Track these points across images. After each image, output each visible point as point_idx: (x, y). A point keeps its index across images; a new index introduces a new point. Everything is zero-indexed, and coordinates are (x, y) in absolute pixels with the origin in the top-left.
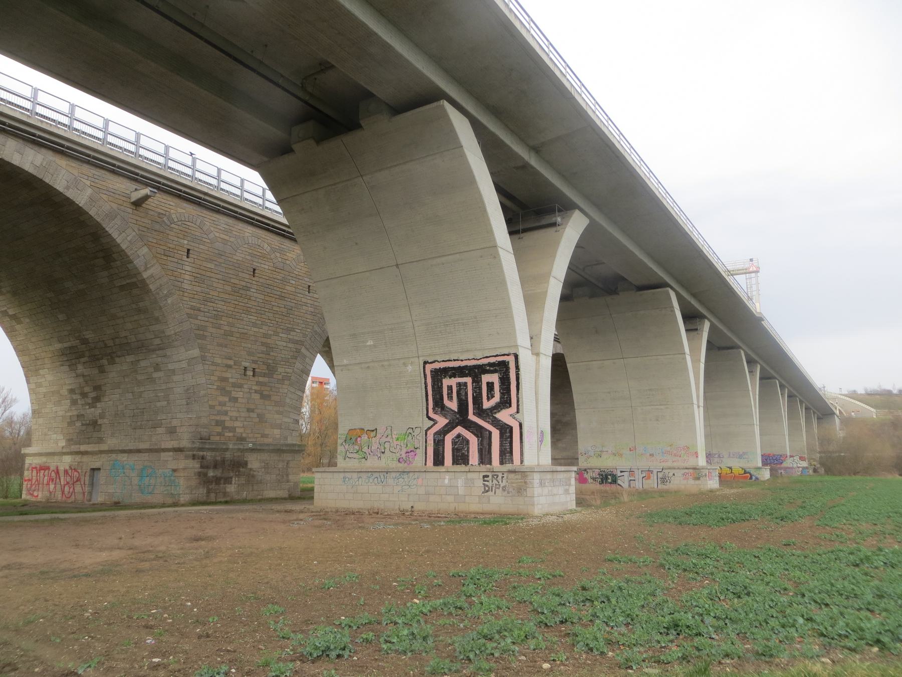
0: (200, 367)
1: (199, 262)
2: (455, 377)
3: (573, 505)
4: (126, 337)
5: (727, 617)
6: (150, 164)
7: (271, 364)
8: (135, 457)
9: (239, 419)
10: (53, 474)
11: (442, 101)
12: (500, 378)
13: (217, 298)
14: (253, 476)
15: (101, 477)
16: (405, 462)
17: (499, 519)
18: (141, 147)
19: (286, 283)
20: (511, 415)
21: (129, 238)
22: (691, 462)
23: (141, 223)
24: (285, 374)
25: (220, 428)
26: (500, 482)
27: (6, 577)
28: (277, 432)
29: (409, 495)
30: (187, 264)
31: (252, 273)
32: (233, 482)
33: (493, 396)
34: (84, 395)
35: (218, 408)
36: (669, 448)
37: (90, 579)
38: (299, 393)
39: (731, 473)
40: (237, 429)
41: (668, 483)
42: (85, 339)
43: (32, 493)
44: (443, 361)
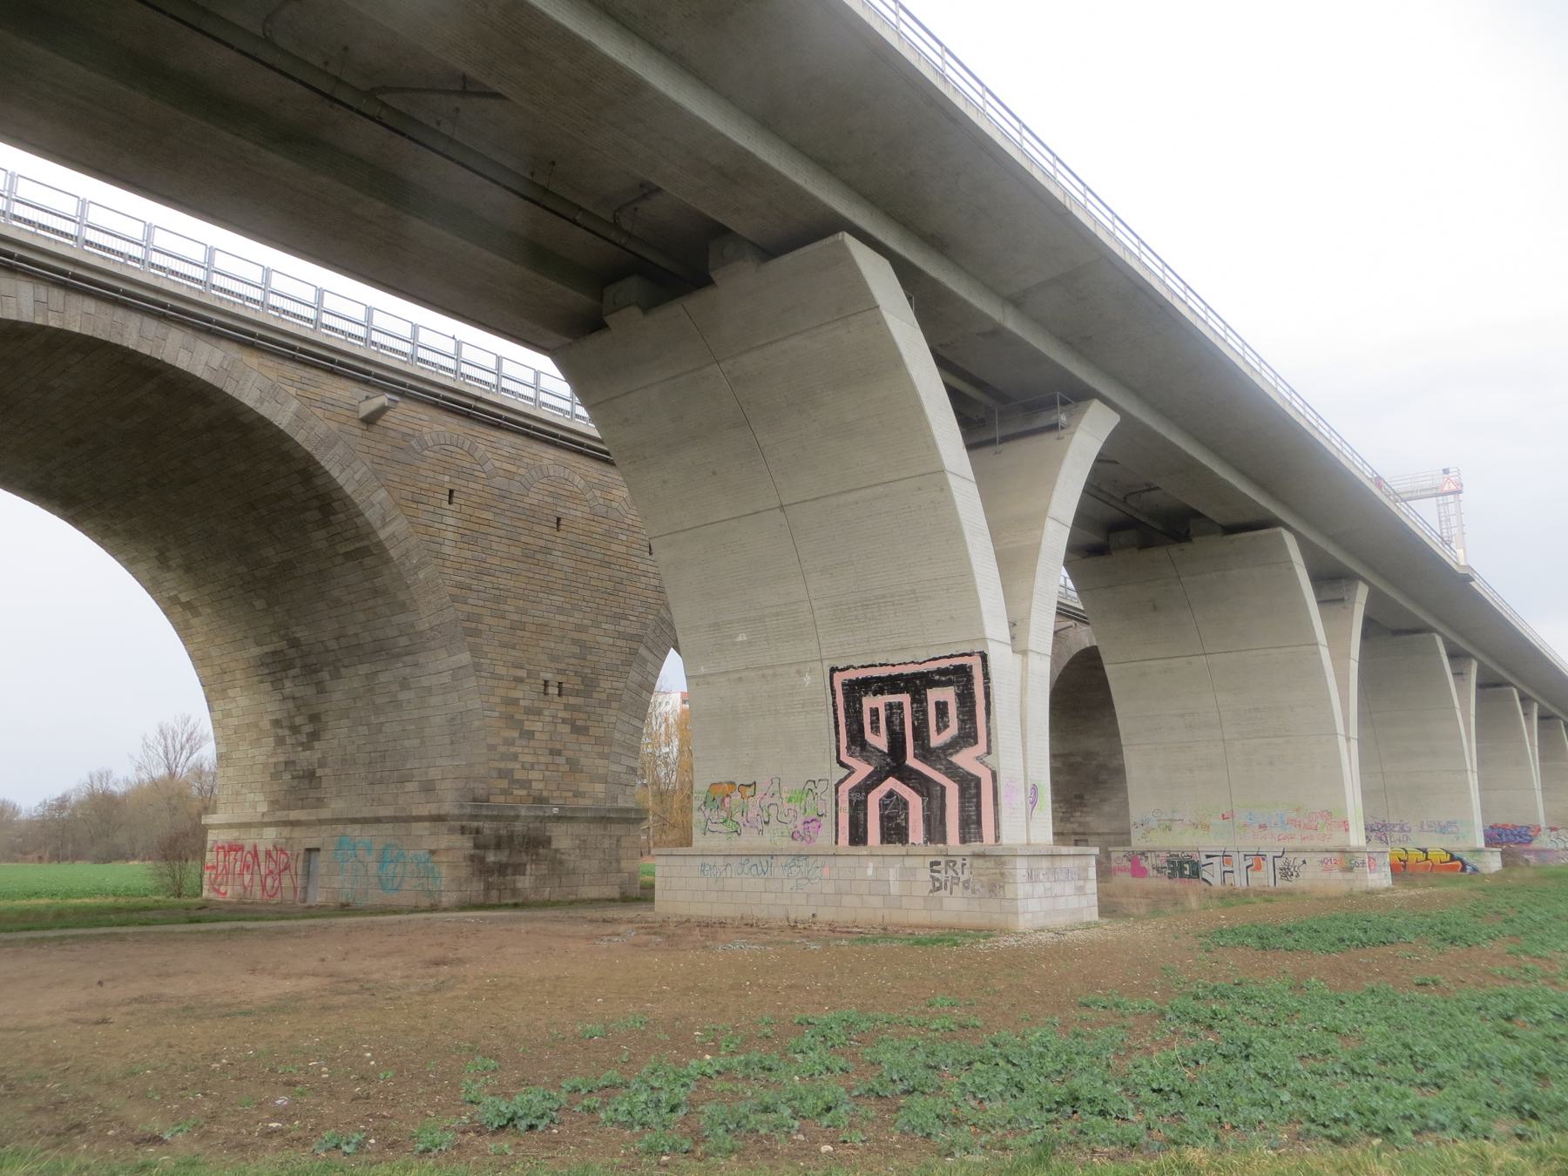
0: (471, 683)
1: (469, 511)
2: (882, 694)
3: (1093, 915)
4: (356, 635)
5: (1173, 1090)
6: (388, 356)
7: (589, 676)
8: (372, 830)
9: (536, 767)
10: (249, 858)
11: (840, 234)
12: (957, 694)
13: (498, 568)
14: (561, 862)
15: (321, 863)
16: (803, 839)
17: (949, 936)
18: (374, 329)
19: (611, 540)
20: (977, 758)
21: (357, 477)
22: (1337, 840)
23: (375, 452)
24: (613, 691)
25: (506, 781)
26: (960, 874)
27: (132, 1014)
28: (600, 788)
29: (808, 895)
30: (450, 513)
31: (555, 526)
32: (528, 872)
33: (946, 726)
34: (295, 729)
35: (502, 749)
36: (1294, 815)
37: (247, 1019)
38: (636, 722)
39: (1427, 859)
40: (533, 783)
41: (1294, 877)
42: (295, 638)
43: (217, 887)
44: (863, 667)
